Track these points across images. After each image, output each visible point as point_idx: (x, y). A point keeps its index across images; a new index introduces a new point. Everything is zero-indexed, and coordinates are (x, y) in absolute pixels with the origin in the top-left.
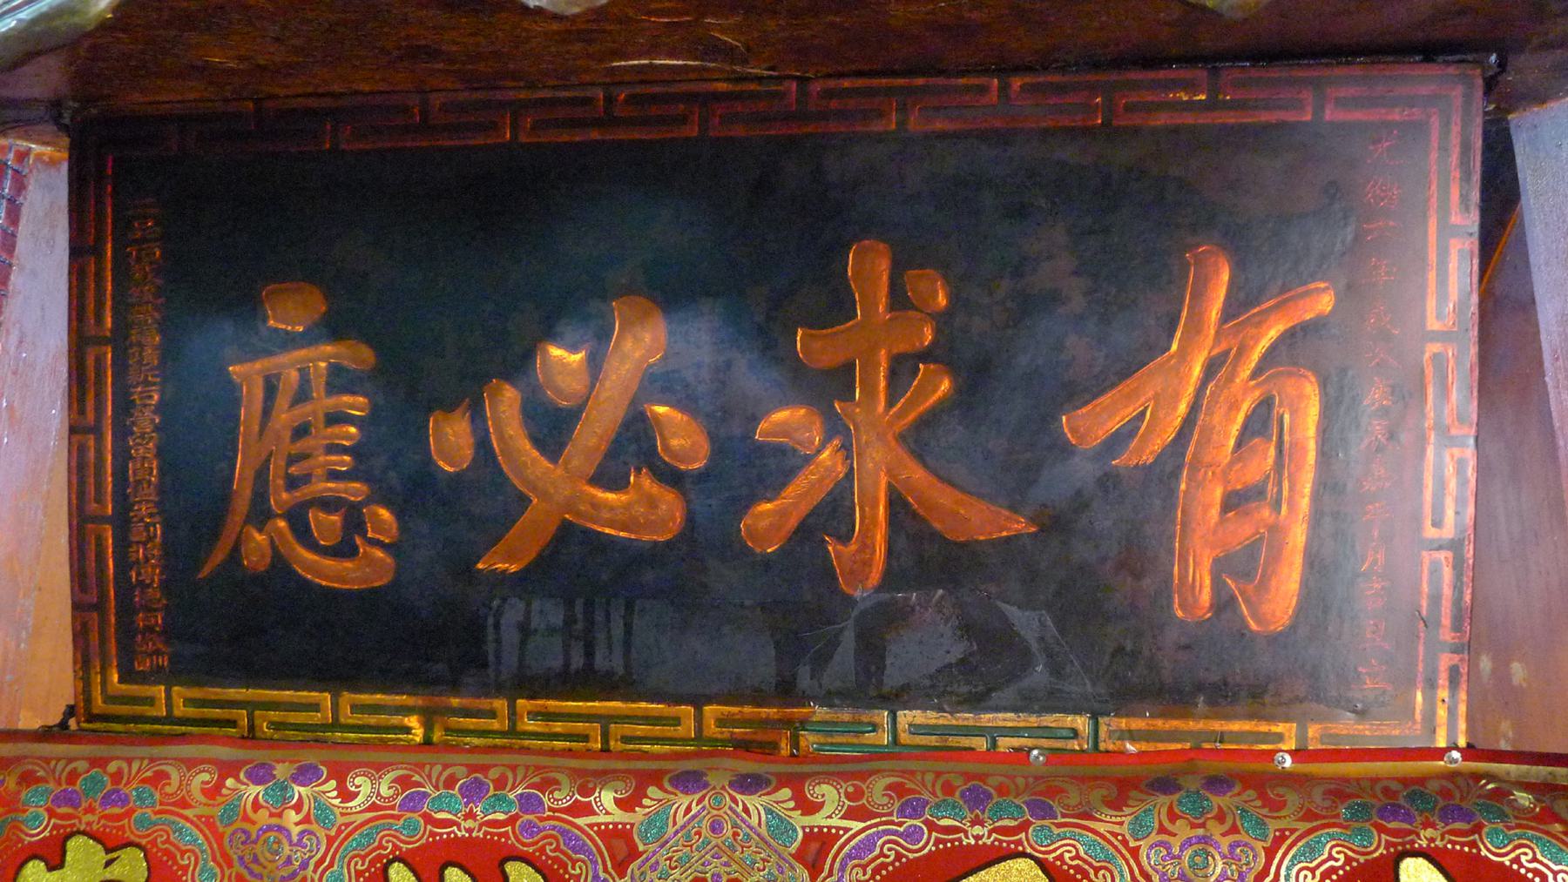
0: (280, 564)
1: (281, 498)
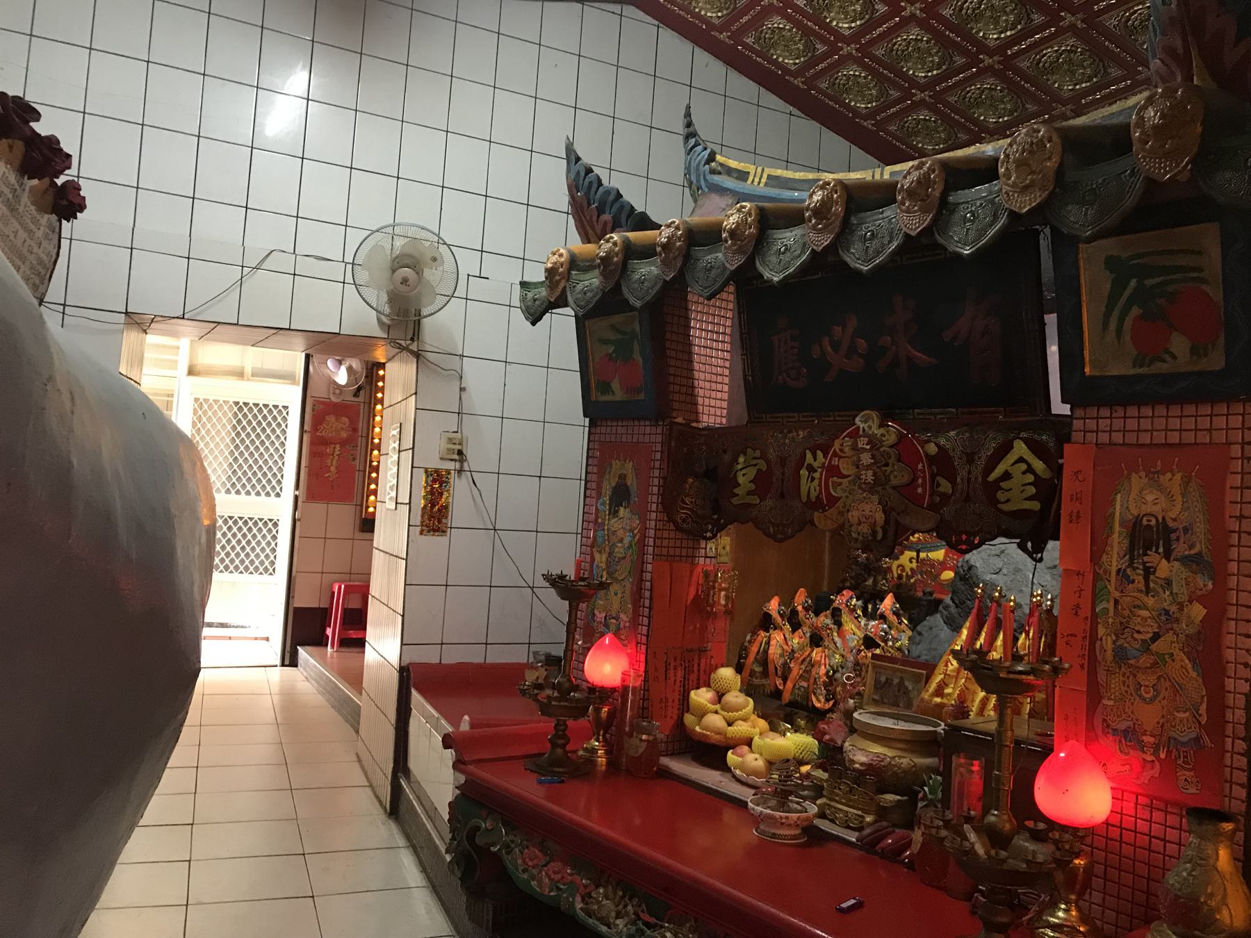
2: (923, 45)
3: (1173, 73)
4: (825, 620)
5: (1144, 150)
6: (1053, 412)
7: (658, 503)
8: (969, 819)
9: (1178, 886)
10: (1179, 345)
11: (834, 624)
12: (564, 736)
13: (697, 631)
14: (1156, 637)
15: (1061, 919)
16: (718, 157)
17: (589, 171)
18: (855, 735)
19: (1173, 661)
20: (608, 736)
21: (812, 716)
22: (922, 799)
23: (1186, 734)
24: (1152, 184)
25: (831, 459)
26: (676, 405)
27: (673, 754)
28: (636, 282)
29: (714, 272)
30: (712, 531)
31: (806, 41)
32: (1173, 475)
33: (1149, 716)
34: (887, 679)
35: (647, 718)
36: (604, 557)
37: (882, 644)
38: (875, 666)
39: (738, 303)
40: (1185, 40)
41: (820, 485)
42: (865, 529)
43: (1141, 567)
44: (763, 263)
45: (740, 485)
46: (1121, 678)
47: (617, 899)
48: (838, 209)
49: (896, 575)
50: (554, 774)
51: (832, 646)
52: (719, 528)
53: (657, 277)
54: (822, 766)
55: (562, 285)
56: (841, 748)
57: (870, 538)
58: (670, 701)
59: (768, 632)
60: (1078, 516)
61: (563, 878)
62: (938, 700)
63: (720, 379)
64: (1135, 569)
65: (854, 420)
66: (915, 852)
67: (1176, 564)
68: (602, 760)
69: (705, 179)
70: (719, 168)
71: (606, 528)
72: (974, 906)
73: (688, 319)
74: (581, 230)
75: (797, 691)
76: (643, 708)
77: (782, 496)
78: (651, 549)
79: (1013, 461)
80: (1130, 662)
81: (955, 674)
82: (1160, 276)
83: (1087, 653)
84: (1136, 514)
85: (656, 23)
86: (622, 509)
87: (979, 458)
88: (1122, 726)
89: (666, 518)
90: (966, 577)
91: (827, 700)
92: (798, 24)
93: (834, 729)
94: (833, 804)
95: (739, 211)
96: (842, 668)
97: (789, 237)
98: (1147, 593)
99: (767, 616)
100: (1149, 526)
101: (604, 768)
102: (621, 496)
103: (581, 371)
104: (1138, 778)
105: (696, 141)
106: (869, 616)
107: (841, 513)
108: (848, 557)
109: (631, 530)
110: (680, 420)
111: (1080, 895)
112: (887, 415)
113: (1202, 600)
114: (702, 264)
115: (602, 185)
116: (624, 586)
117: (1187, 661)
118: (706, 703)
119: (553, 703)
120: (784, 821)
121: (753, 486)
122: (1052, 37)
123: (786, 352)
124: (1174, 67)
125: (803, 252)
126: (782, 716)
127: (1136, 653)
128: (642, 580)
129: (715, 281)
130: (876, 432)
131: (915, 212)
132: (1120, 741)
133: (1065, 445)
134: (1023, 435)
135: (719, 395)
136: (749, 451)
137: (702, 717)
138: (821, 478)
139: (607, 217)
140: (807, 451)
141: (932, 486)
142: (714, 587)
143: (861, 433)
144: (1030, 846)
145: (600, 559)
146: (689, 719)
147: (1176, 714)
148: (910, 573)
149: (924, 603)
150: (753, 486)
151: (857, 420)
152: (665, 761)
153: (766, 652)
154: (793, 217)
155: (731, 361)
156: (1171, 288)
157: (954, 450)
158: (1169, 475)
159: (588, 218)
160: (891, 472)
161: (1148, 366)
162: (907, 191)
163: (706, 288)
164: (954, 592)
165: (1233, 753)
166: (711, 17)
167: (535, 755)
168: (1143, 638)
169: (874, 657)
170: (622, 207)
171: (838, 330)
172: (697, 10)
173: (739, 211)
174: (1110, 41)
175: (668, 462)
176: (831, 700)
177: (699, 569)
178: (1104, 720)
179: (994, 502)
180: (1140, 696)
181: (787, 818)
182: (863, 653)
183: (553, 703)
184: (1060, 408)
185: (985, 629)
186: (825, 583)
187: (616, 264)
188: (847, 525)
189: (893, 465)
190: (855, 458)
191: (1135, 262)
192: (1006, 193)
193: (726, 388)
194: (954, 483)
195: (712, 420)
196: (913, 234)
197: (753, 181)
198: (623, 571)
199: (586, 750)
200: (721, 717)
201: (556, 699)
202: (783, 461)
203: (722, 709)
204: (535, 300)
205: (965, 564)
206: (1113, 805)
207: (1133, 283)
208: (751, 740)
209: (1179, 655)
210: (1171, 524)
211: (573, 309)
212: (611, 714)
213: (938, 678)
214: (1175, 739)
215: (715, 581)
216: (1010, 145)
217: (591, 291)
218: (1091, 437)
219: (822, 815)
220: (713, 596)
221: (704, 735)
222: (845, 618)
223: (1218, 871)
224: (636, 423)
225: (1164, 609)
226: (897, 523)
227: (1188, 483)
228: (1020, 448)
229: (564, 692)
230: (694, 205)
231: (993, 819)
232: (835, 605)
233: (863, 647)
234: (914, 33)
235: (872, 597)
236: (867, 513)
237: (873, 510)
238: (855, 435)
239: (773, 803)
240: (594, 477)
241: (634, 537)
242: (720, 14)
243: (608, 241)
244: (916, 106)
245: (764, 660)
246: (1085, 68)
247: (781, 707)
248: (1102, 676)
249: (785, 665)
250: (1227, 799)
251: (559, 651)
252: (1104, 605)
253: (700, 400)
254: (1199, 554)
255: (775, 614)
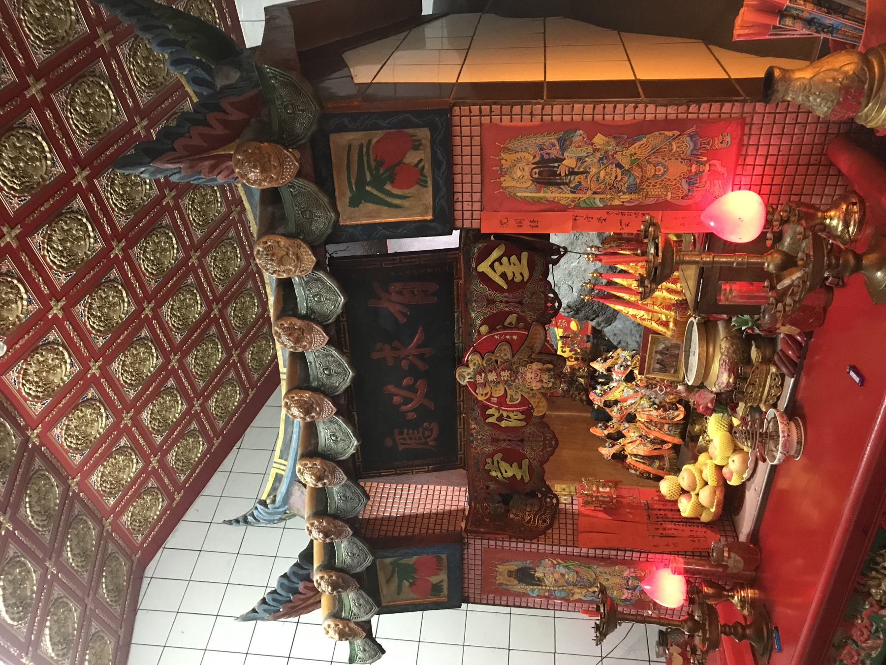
0: (434, 440)
1: (423, 440)
2: (200, 354)
3: (227, 167)
4: (614, 412)
5: (277, 180)
6: (457, 246)
7: (531, 543)
8: (772, 288)
9: (829, 104)
10: (412, 158)
11: (617, 405)
12: (735, 627)
13: (633, 511)
14: (619, 166)
15: (839, 221)
16: (263, 498)
17: (264, 601)
18: (705, 384)
19: (635, 154)
20: (727, 588)
21: (691, 421)
22: (753, 330)
23: (687, 144)
24: (299, 174)
25: (494, 403)
26: (451, 528)
27: (735, 532)
28: (353, 560)
29: (348, 494)
30: (552, 499)
31: (188, 436)
32: (503, 159)
33: (677, 169)
34: (657, 363)
35: (709, 553)
36: (577, 590)
37: (630, 368)
38: (648, 372)
39: (372, 477)
40: (206, 159)
41: (513, 411)
42: (545, 377)
43: (569, 177)
44: (342, 454)
45: (514, 475)
46: (651, 187)
47: (880, 576)
48: (307, 395)
49: (576, 362)
50: (770, 636)
51: (634, 407)
52: (549, 491)
53: (349, 542)
54: (734, 409)
55: (352, 625)
56: (717, 394)
57: (552, 373)
58: (692, 534)
59: (626, 456)
60: (533, 221)
61: (866, 627)
62: (671, 325)
63: (431, 492)
64: (570, 181)
65: (464, 386)
66: (799, 331)
67: (566, 154)
68: (750, 593)
69: (279, 508)
70: (271, 497)
71: (552, 589)
72: (837, 285)
73: (383, 519)
74: (310, 609)
75: (672, 433)
76: (701, 556)
77: (522, 441)
78: (569, 549)
79: (493, 272)
80: (638, 182)
81: (650, 313)
82: (364, 171)
83: (634, 212)
84: (531, 182)
85: (161, 549)
86: (536, 574)
87: (491, 295)
88: (686, 186)
89: (543, 536)
90: (577, 310)
91: (677, 409)
92: (150, 399)
93: (702, 400)
94: (764, 398)
95: (302, 474)
96: (651, 398)
97: (324, 434)
98: (589, 173)
99: (615, 456)
100: (540, 173)
101: (757, 591)
102: (526, 576)
103: (423, 610)
104: (723, 174)
105: (250, 515)
106: (608, 379)
107: (534, 396)
108: (564, 396)
109: (554, 566)
110: (463, 525)
111: (818, 210)
112: (459, 362)
113: (591, 137)
114: (341, 504)
115: (275, 590)
116: (601, 572)
117: (635, 145)
118: (691, 503)
119: (708, 636)
120: (786, 435)
121: (515, 465)
122: (204, 271)
123: (411, 439)
124: (223, 166)
125: (336, 422)
126: (693, 444)
127: (631, 179)
128: (595, 557)
129: (355, 493)
130: (472, 369)
131: (311, 337)
132: (697, 187)
133: (482, 232)
134: (474, 265)
135: (443, 493)
136: (487, 467)
137: (703, 506)
138: (507, 411)
139: (301, 586)
140: (487, 421)
141: (512, 329)
142: (597, 497)
143: (472, 380)
144: (787, 240)
145: (579, 593)
146: (705, 518)
147: (674, 151)
148: (573, 352)
149: (595, 341)
150: (515, 465)
151: (462, 383)
152: (743, 538)
153: (643, 457)
154: (310, 430)
155: (417, 483)
156: (373, 164)
157: (485, 313)
158: (503, 162)
159: (301, 602)
160: (502, 358)
161: (427, 177)
162: (295, 344)
163: (360, 501)
164: (587, 318)
165: (698, 113)
166: (162, 507)
167: (754, 655)
168: (620, 174)
169: (641, 373)
170: (294, 573)
171: (396, 399)
172: (155, 517)
173: (302, 474)
174: (211, 236)
175: (497, 534)
176: (676, 406)
177: (583, 509)
178: (682, 198)
179: (523, 283)
180: (663, 175)
181: (783, 432)
182: (639, 383)
183: (708, 636)
184: (452, 241)
185: (615, 293)
186: (584, 415)
187: (337, 577)
188: (543, 391)
189: (496, 357)
190: (492, 385)
191: (354, 187)
192: (301, 272)
193: (438, 487)
194: (510, 313)
195: (462, 498)
196: (327, 339)
197: (283, 470)
198: (588, 574)
199: (742, 607)
200: (701, 491)
201: (704, 634)
202: (495, 440)
203: (694, 489)
204: (365, 650)
205: (566, 311)
206: (745, 189)
207: (368, 188)
208: (717, 466)
209: (632, 149)
210: (538, 159)
211: (372, 616)
212: (710, 584)
213: (655, 326)
214: (692, 151)
215: (592, 496)
216: (267, 270)
217: (358, 599)
218: (476, 215)
219: (775, 406)
220: (604, 497)
221: (717, 505)
222: (611, 397)
223: (814, 76)
224: (466, 562)
225: (599, 161)
226: (540, 353)
227: (509, 150)
228: (484, 267)
229: (696, 627)
230: (297, 517)
231: (771, 267)
232: (602, 405)
233: (634, 383)
234: (190, 360)
235: (593, 378)
236: (533, 375)
237: (531, 371)
238: (474, 385)
239: (771, 445)
240: (511, 599)
241: (559, 564)
242: (161, 500)
243: (319, 584)
244: (241, 360)
245: (649, 459)
246: (227, 251)
247: (686, 445)
248: (651, 201)
249: (653, 442)
250: (733, 115)
251: (654, 629)
252: (597, 201)
253: (447, 508)
254: (558, 140)
255: (613, 451)
